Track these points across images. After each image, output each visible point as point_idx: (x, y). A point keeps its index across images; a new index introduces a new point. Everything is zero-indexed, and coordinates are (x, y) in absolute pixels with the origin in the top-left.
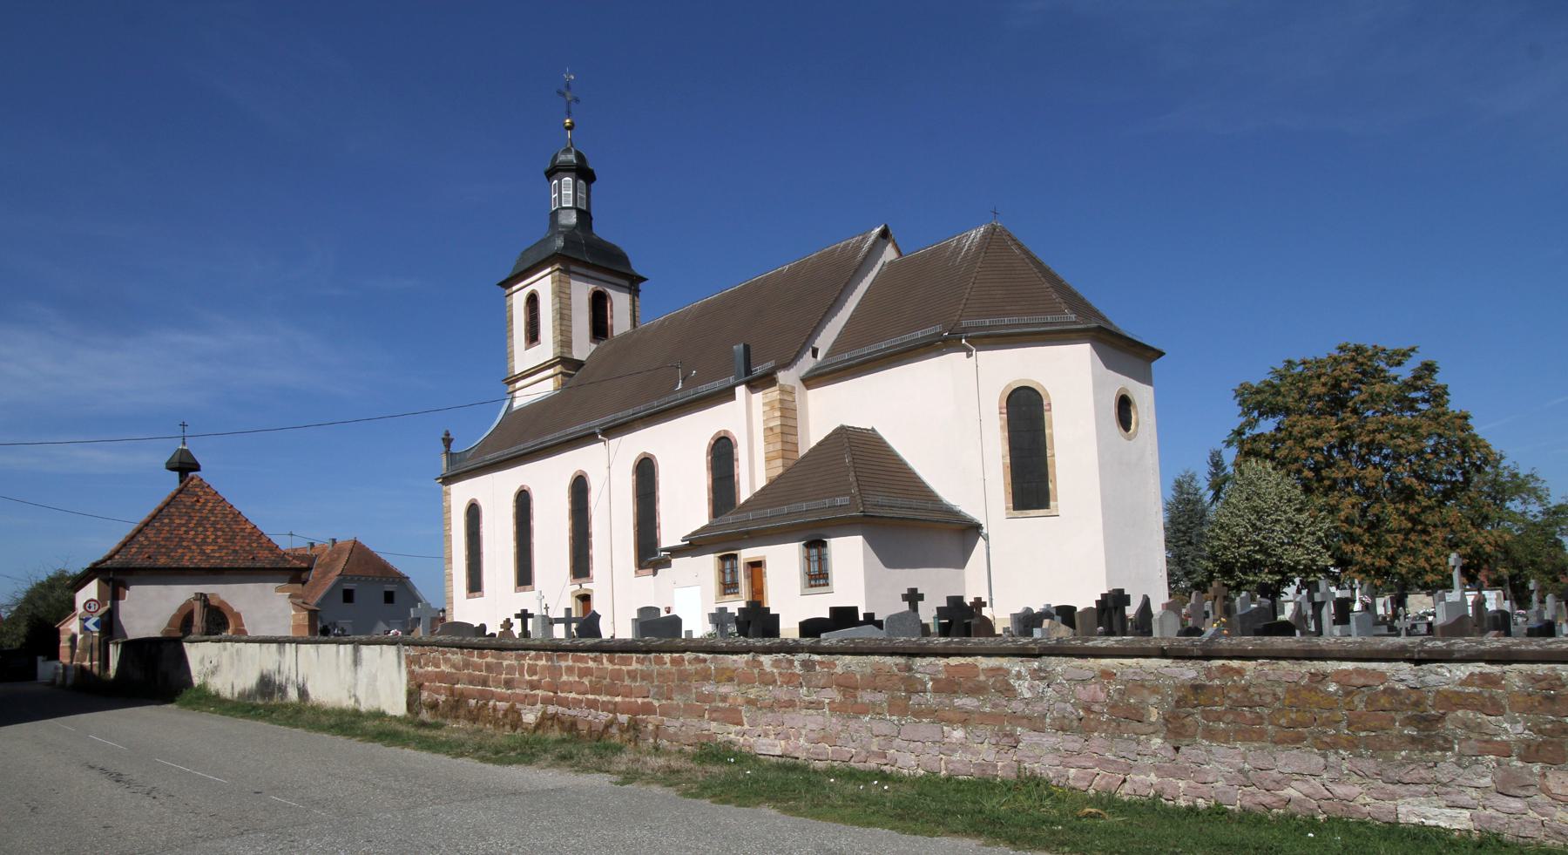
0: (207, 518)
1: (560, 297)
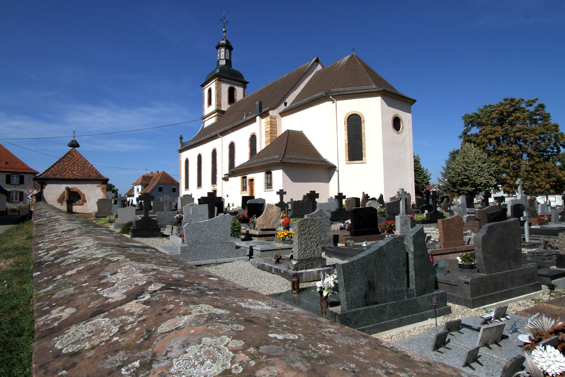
0: (76, 162)
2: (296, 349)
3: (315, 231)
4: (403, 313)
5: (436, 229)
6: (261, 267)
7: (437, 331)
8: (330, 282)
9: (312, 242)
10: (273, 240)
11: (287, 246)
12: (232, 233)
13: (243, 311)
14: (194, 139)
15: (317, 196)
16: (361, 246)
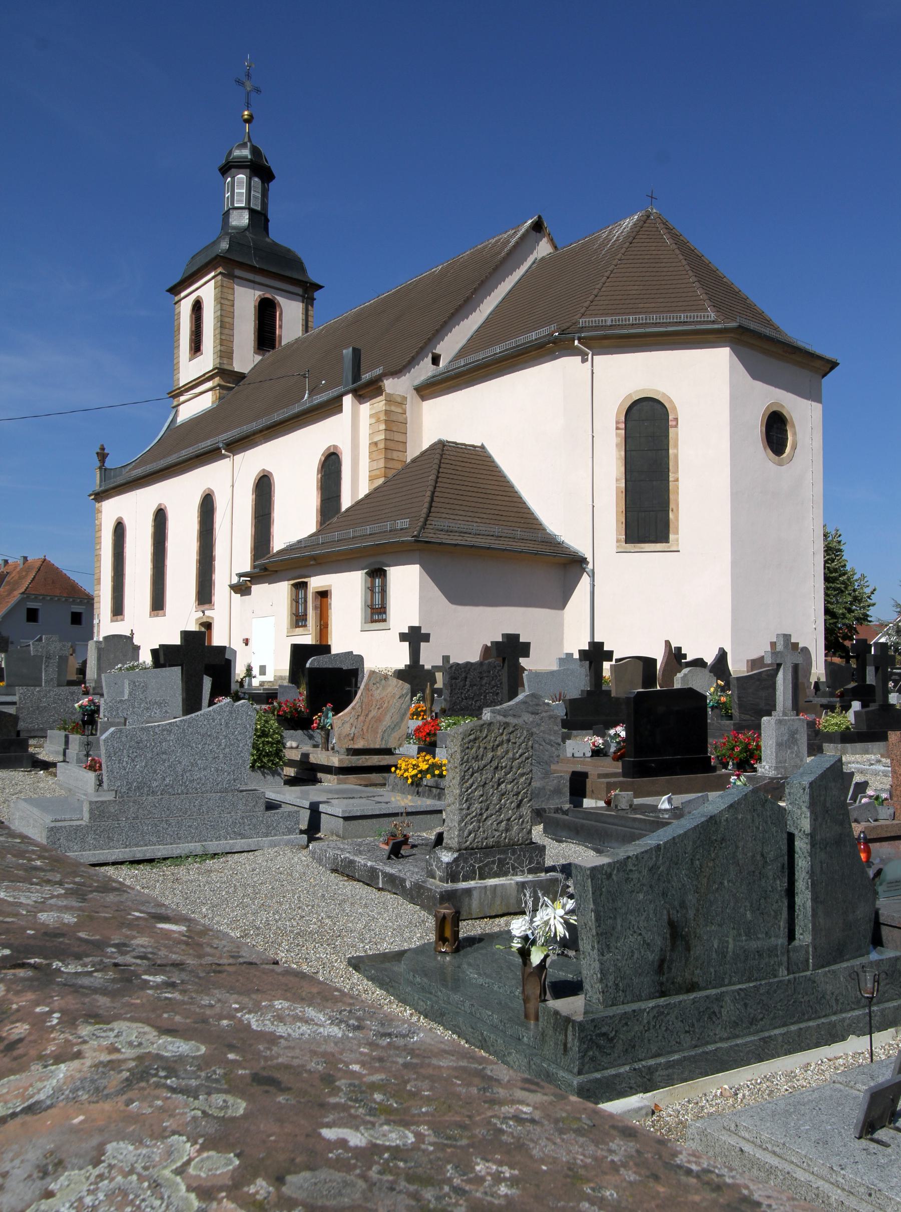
1: (221, 304)
2: (403, 1184)
3: (514, 759)
4: (774, 1018)
5: (884, 760)
6: (345, 867)
7: (872, 1078)
8: (552, 922)
9: (503, 795)
10: (384, 785)
11: (427, 803)
12: (255, 761)
13: (251, 1045)
14: (143, 461)
15: (525, 649)
16: (654, 809)
